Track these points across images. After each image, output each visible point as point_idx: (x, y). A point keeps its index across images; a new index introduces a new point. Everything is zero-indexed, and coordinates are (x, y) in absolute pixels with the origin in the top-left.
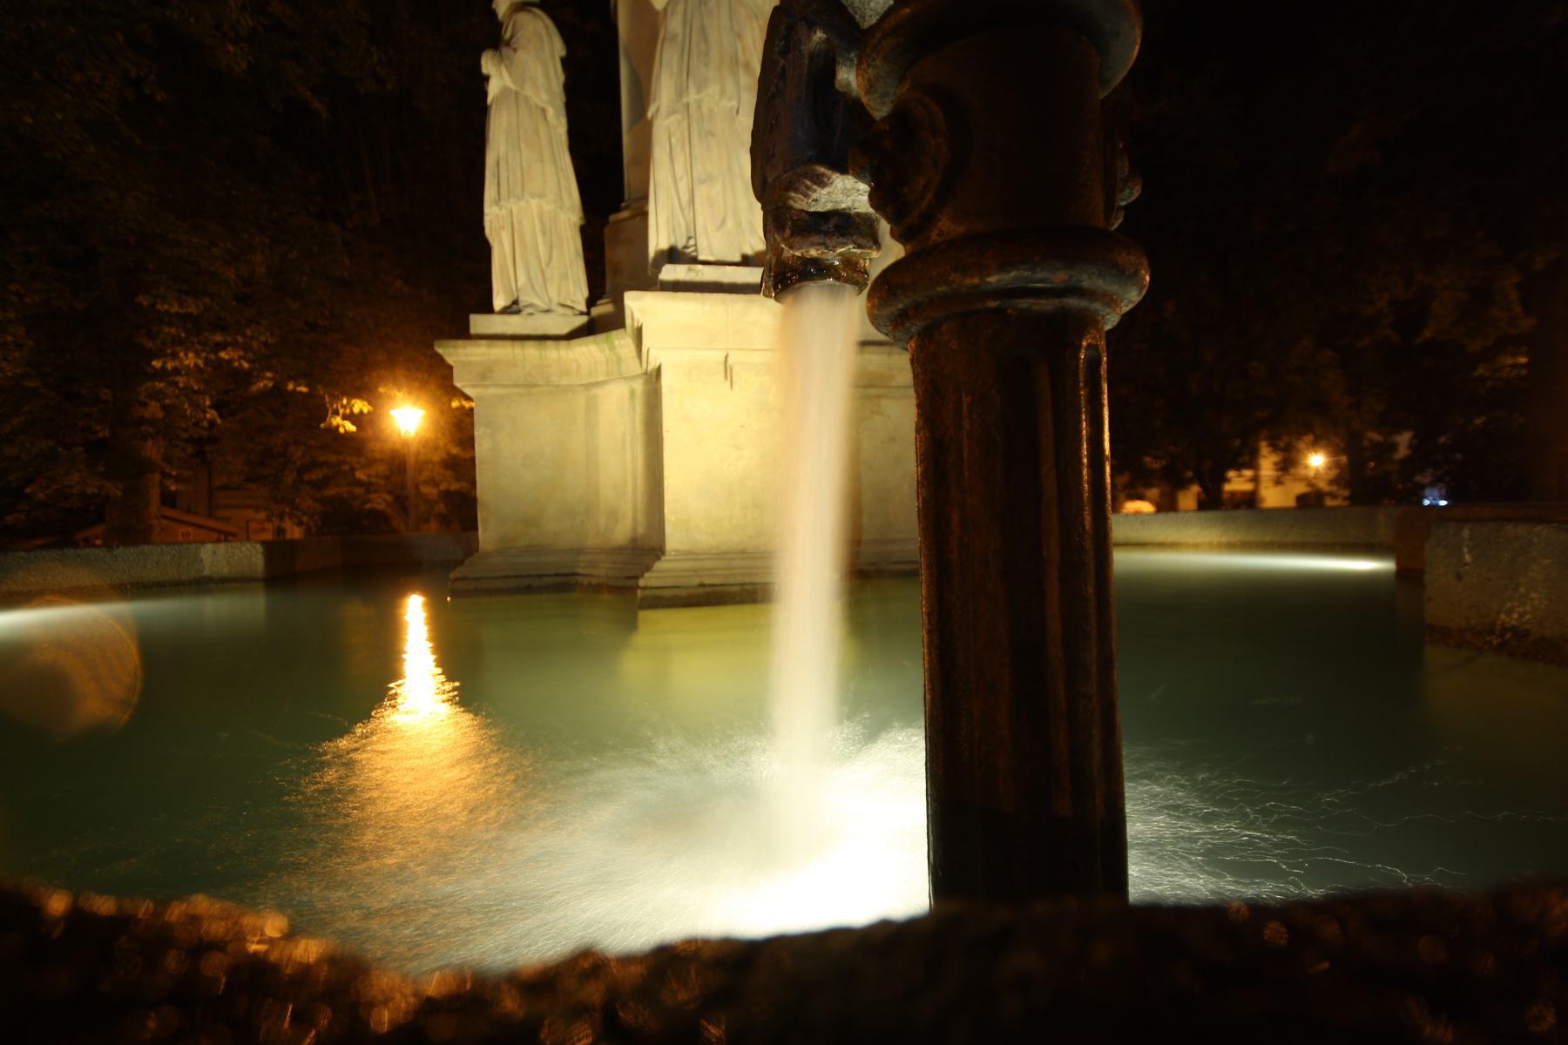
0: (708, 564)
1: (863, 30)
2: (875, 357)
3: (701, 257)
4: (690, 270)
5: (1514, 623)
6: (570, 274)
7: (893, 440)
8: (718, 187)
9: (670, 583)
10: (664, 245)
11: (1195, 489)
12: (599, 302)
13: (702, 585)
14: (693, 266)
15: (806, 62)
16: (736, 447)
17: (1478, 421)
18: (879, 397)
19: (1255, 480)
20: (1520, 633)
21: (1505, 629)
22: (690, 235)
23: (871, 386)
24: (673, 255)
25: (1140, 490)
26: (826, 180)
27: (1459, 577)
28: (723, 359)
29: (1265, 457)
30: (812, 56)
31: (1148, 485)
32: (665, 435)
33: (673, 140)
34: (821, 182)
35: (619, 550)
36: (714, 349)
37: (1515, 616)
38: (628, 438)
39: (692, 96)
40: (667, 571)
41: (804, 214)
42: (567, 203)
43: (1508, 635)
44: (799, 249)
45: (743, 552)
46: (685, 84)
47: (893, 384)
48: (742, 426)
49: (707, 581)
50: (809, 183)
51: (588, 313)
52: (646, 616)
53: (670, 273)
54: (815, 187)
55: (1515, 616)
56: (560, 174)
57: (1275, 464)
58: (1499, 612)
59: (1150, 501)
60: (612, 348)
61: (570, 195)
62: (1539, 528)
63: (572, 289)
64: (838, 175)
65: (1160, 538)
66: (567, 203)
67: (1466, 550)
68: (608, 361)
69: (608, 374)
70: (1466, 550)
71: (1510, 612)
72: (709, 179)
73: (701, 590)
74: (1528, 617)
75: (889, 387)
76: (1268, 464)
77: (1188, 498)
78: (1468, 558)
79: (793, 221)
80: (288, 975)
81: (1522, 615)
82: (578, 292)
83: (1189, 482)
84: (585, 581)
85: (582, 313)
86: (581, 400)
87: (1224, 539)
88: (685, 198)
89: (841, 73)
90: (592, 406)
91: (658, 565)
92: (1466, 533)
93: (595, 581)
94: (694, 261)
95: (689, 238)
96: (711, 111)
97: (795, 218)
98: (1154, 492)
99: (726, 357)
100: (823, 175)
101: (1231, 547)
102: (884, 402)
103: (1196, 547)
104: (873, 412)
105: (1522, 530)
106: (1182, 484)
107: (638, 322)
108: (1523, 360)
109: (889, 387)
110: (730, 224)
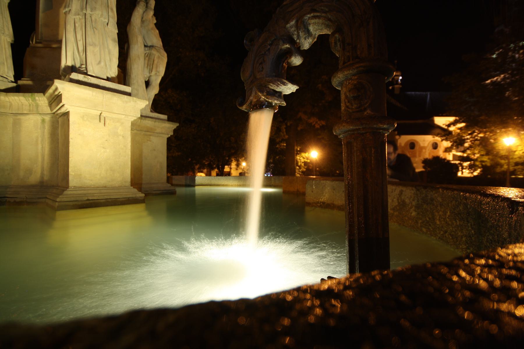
0: (90, 192)
1: (301, 50)
2: (149, 122)
3: (89, 73)
4: (85, 77)
5: (323, 201)
6: (5, 63)
7: (154, 150)
8: (97, 49)
9: (73, 199)
10: (70, 63)
11: (216, 170)
12: (22, 79)
13: (88, 200)
14: (86, 76)
15: (279, 50)
16: (104, 148)
17: (277, 157)
18: (150, 135)
19: (231, 168)
20: (323, 203)
21: (321, 202)
22: (82, 63)
23: (148, 131)
24: (73, 69)
25: (202, 170)
26: (286, 84)
27: (312, 192)
28: (99, 114)
29: (233, 163)
30: (281, 50)
31: (204, 169)
32: (70, 140)
33: (77, 25)
34: (284, 84)
35: (33, 186)
36: (96, 110)
37: (323, 199)
38: (40, 139)
39: (89, 12)
40: (70, 194)
41: (271, 90)
42: (7, 32)
43: (321, 204)
44: (271, 99)
45: (105, 187)
46: (85, 6)
47: (156, 132)
48: (106, 140)
49: (90, 198)
50: (279, 83)
51: (16, 82)
52: (58, 213)
53: (74, 76)
54: (281, 85)
55: (323, 199)
56: (4, 19)
57: (236, 165)
58: (320, 199)
59: (204, 173)
60: (34, 100)
61: (9, 30)
62: (327, 181)
63: (6, 70)
64: (291, 84)
65: (223, 184)
66: (7, 32)
67: (314, 186)
68: (30, 105)
69: (30, 111)
70: (314, 186)
71: (322, 199)
72: (94, 45)
73: (88, 202)
74: (325, 199)
75: (154, 133)
76: (234, 165)
77: (214, 173)
78: (314, 187)
79: (267, 91)
80: (352, 270)
81: (324, 199)
82: (10, 74)
83: (215, 168)
84: (12, 200)
85: (12, 82)
86: (11, 120)
87: (239, 184)
88: (81, 48)
89: (293, 58)
90: (17, 124)
91: (65, 192)
92: (314, 182)
93: (18, 200)
94: (86, 74)
95: (82, 65)
96: (96, 20)
97: (268, 90)
98: (205, 170)
99: (101, 114)
100: (285, 82)
101: (240, 186)
102: (151, 137)
103: (232, 186)
104: (147, 140)
105: (324, 182)
106: (213, 169)
107: (60, 92)
108: (285, 145)
109: (154, 133)
110: (102, 64)
